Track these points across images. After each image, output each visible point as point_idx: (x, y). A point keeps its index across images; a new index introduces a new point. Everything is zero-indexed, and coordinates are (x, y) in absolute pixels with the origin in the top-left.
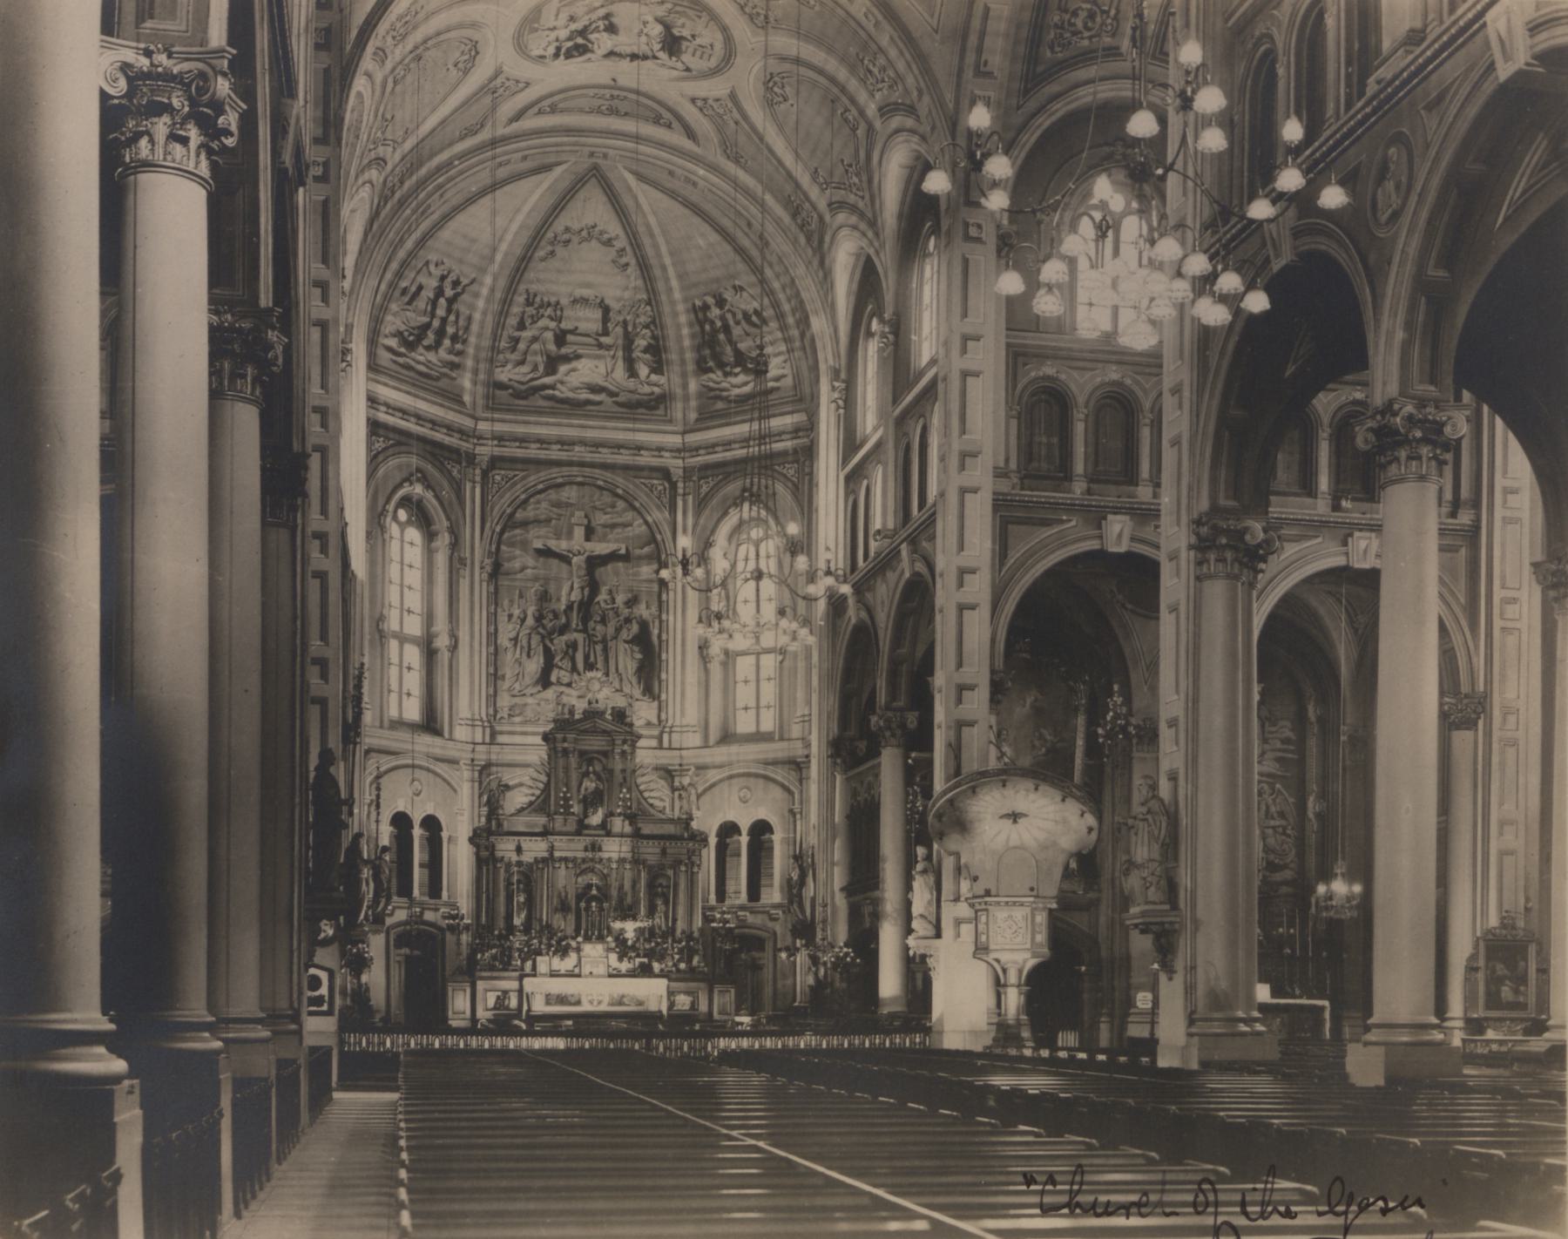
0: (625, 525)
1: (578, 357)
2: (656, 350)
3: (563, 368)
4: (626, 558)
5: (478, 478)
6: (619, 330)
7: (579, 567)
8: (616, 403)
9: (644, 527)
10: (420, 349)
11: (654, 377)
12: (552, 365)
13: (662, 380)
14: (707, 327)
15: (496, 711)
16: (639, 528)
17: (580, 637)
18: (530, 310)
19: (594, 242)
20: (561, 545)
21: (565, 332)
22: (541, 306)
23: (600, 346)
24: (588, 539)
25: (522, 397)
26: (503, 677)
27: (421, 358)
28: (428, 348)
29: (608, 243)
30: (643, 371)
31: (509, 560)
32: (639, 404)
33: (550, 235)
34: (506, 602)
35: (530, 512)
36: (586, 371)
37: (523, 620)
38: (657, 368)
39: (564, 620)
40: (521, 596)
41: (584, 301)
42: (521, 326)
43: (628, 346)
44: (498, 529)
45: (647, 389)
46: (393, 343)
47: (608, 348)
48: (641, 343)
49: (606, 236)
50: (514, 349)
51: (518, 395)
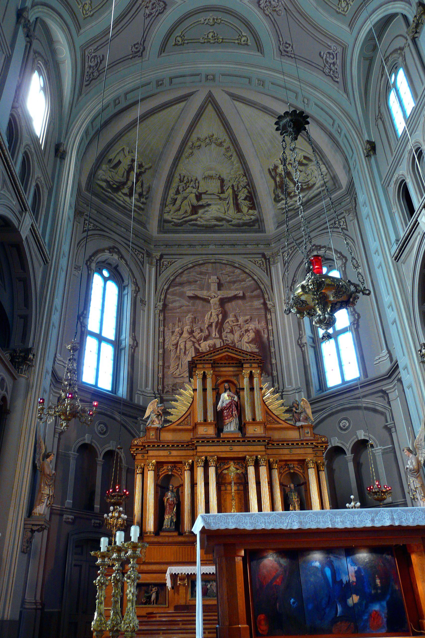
0: (241, 281)
1: (209, 205)
2: (252, 198)
3: (201, 211)
4: (243, 298)
5: (154, 263)
6: (230, 191)
7: (215, 304)
8: (230, 225)
9: (252, 282)
10: (120, 193)
11: (251, 211)
12: (195, 210)
13: (256, 212)
14: (278, 179)
15: (163, 387)
16: (249, 282)
18: (182, 184)
19: (213, 145)
20: (204, 294)
21: (201, 194)
22: (188, 182)
23: (220, 199)
24: (219, 289)
25: (178, 227)
26: (169, 367)
27: (121, 199)
28: (125, 194)
29: (221, 145)
30: (245, 209)
31: (173, 302)
32: (244, 224)
33: (190, 144)
34: (170, 325)
35: (184, 278)
36: (214, 210)
37: (181, 334)
38: (253, 206)
39: (207, 332)
40: (179, 321)
41: (211, 177)
42: (178, 192)
43: (235, 197)
44: (166, 287)
45: (248, 217)
46: (104, 184)
47: (225, 199)
48: (242, 195)
49: (220, 141)
50: (174, 204)
51: (176, 225)
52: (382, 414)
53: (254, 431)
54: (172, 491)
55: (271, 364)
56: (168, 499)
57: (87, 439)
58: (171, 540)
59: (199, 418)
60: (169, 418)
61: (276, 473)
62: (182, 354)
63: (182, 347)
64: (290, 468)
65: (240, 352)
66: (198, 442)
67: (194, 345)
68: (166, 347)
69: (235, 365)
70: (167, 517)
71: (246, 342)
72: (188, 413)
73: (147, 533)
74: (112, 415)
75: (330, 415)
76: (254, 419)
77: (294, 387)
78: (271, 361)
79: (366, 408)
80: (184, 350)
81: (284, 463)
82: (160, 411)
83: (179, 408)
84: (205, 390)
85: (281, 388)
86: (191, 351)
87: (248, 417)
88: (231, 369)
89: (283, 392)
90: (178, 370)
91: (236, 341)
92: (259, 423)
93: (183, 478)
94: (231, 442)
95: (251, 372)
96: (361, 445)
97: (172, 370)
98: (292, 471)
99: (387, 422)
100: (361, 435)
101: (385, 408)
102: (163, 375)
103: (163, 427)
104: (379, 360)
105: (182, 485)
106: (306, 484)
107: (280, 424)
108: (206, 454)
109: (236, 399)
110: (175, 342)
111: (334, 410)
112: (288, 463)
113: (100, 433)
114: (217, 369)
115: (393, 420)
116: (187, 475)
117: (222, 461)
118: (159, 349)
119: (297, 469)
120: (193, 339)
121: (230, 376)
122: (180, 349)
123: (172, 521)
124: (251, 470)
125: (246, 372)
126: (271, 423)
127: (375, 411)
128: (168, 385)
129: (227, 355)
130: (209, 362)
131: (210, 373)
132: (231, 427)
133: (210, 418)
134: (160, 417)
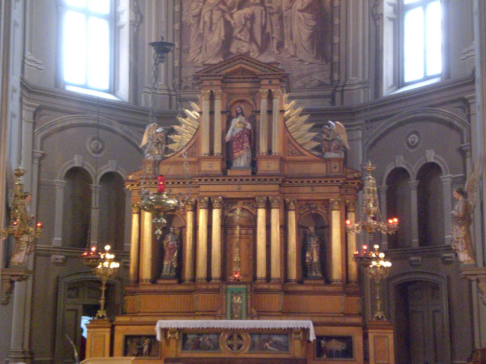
15: (181, 81)
17: (258, 10)
26: (188, 50)
52: (459, 130)
53: (267, 166)
54: (174, 234)
55: (332, 44)
56: (168, 242)
57: (77, 162)
58: (169, 288)
59: (205, 149)
60: (170, 146)
61: (292, 216)
62: (207, 29)
63: (207, 19)
64: (311, 209)
65: (256, 64)
66: (200, 180)
67: (223, 16)
68: (184, 19)
69: (251, 80)
70: (166, 263)
71: (299, 10)
72: (193, 141)
73: (142, 281)
74: (110, 126)
75: (400, 124)
76: (270, 152)
77: (360, 79)
78: (332, 40)
79: (440, 121)
80: (208, 24)
81: (305, 202)
82: (159, 139)
83: (184, 134)
84: (212, 113)
85: (343, 79)
86: (218, 26)
87: (263, 148)
88: (247, 85)
89: (344, 86)
90: (201, 55)
91: (284, 8)
92: (275, 158)
93: (185, 218)
94: (241, 180)
95: (270, 91)
96: (430, 171)
97: (192, 54)
98: (314, 212)
99: (463, 143)
100: (431, 156)
101: (464, 124)
102: (180, 63)
103: (164, 159)
104: (468, 55)
105: (185, 227)
106: (328, 227)
107: (304, 155)
108: (210, 194)
109: (249, 126)
110: (196, 11)
111: (403, 119)
112: (310, 202)
113: (94, 152)
114: (229, 85)
115: (470, 141)
116: (189, 216)
117: (227, 204)
118: (174, 23)
119: (320, 209)
120: (222, 7)
121: (244, 94)
122: (205, 23)
123: (172, 267)
124: (261, 213)
125: (264, 91)
126: (293, 154)
127: (451, 125)
128: (187, 78)
129: (242, 68)
130: (217, 78)
131: (218, 91)
132: (242, 160)
133: (218, 149)
134: (160, 146)
